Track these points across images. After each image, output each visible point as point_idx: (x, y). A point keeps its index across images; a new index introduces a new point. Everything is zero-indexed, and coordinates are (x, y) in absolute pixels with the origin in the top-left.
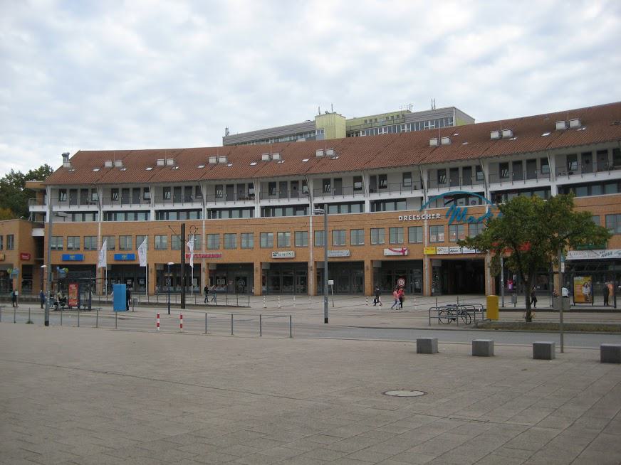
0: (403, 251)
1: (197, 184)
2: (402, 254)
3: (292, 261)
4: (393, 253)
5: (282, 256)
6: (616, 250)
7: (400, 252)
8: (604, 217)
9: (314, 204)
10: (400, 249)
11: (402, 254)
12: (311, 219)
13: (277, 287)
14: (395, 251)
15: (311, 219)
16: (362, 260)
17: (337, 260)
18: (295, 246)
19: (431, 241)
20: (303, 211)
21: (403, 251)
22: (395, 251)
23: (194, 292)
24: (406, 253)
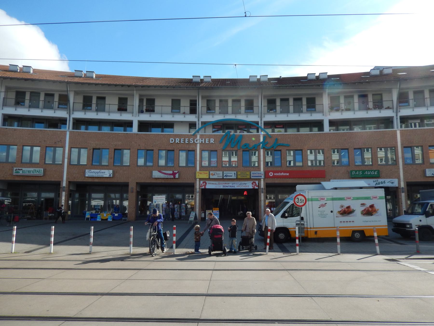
0: (174, 174)
1: (63, 88)
2: (172, 177)
3: (41, 179)
4: (162, 176)
5: (27, 174)
6: (389, 180)
7: (170, 174)
8: (113, 150)
9: (74, 119)
10: (171, 172)
11: (172, 177)
12: (68, 134)
13: (217, 214)
14: (165, 174)
15: (68, 134)
16: (127, 181)
17: (96, 180)
18: (92, 164)
19: (203, 165)
20: (348, 127)
21: (174, 174)
22: (165, 174)
23: (45, 218)
24: (177, 176)
